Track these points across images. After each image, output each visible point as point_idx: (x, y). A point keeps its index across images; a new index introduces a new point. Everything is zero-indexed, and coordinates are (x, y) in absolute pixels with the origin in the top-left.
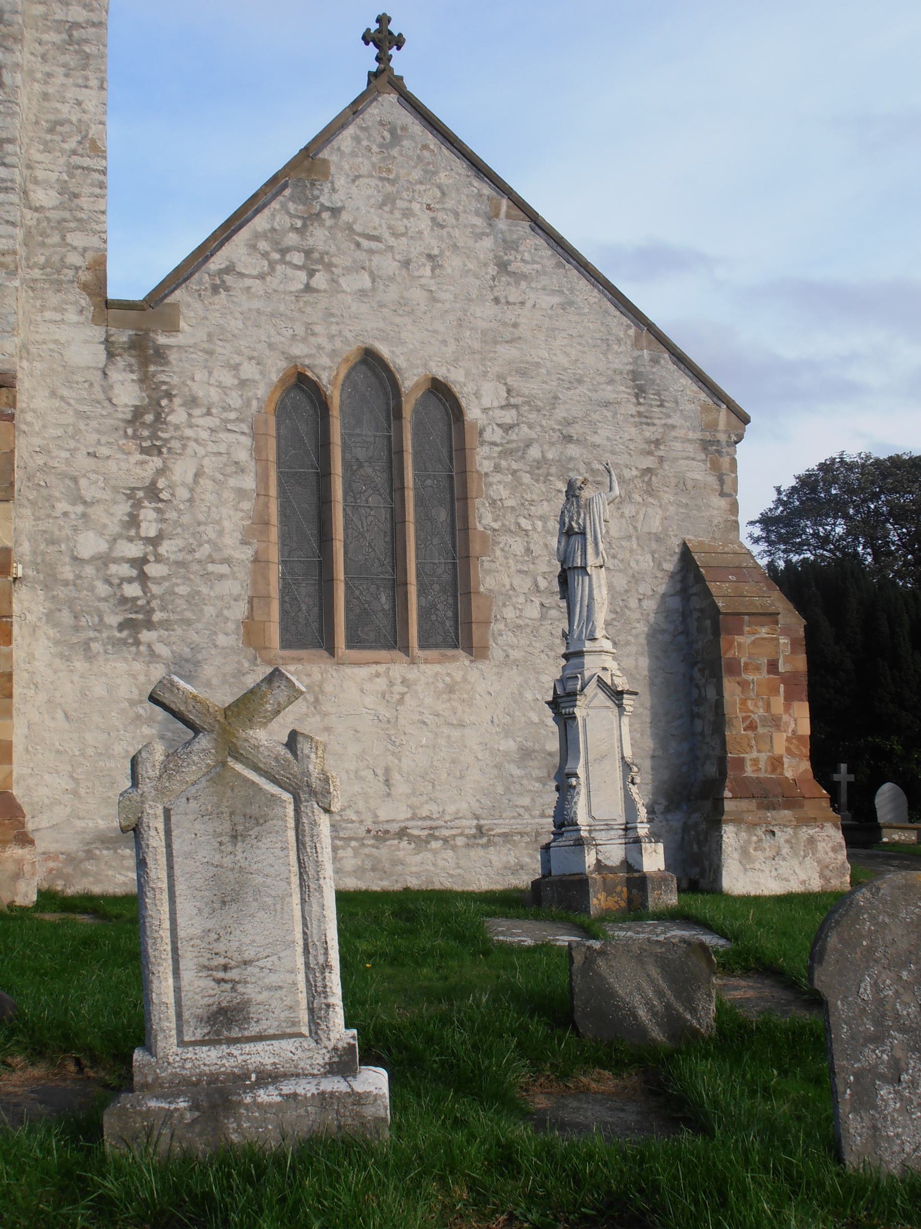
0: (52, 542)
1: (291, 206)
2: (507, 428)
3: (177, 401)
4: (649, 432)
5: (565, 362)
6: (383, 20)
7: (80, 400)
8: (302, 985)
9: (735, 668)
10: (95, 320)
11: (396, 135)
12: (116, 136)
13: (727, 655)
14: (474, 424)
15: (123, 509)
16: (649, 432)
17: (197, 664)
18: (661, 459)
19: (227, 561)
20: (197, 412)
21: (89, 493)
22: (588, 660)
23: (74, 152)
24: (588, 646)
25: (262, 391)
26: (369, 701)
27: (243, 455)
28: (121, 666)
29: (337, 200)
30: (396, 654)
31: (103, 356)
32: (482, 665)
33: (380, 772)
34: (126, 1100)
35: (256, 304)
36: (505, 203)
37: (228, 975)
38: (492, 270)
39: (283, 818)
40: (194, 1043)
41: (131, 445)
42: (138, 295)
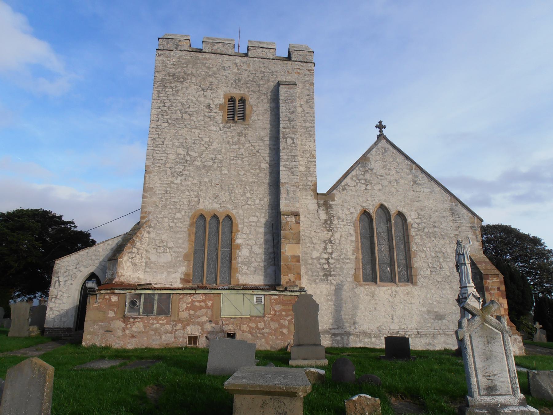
0: (306, 254)
1: (361, 169)
2: (418, 224)
3: (335, 218)
4: (456, 224)
5: (432, 206)
6: (380, 122)
7: (312, 218)
8: (509, 381)
9: (488, 289)
10: (315, 198)
11: (386, 150)
12: (318, 154)
13: (485, 286)
14: (410, 223)
15: (323, 245)
16: (456, 224)
17: (343, 286)
18: (460, 231)
19: (349, 259)
20: (340, 221)
21: (315, 241)
22: (468, 288)
23: (309, 158)
24: (468, 285)
25: (356, 215)
26: (387, 296)
27: (352, 232)
28: (324, 286)
29: (372, 167)
30: (392, 283)
31: (317, 207)
32: (416, 287)
33: (390, 316)
34: (469, 409)
35: (353, 193)
36: (414, 166)
37: (490, 378)
38: (412, 183)
39: (500, 338)
40: (483, 395)
41: (324, 229)
42: (325, 191)
